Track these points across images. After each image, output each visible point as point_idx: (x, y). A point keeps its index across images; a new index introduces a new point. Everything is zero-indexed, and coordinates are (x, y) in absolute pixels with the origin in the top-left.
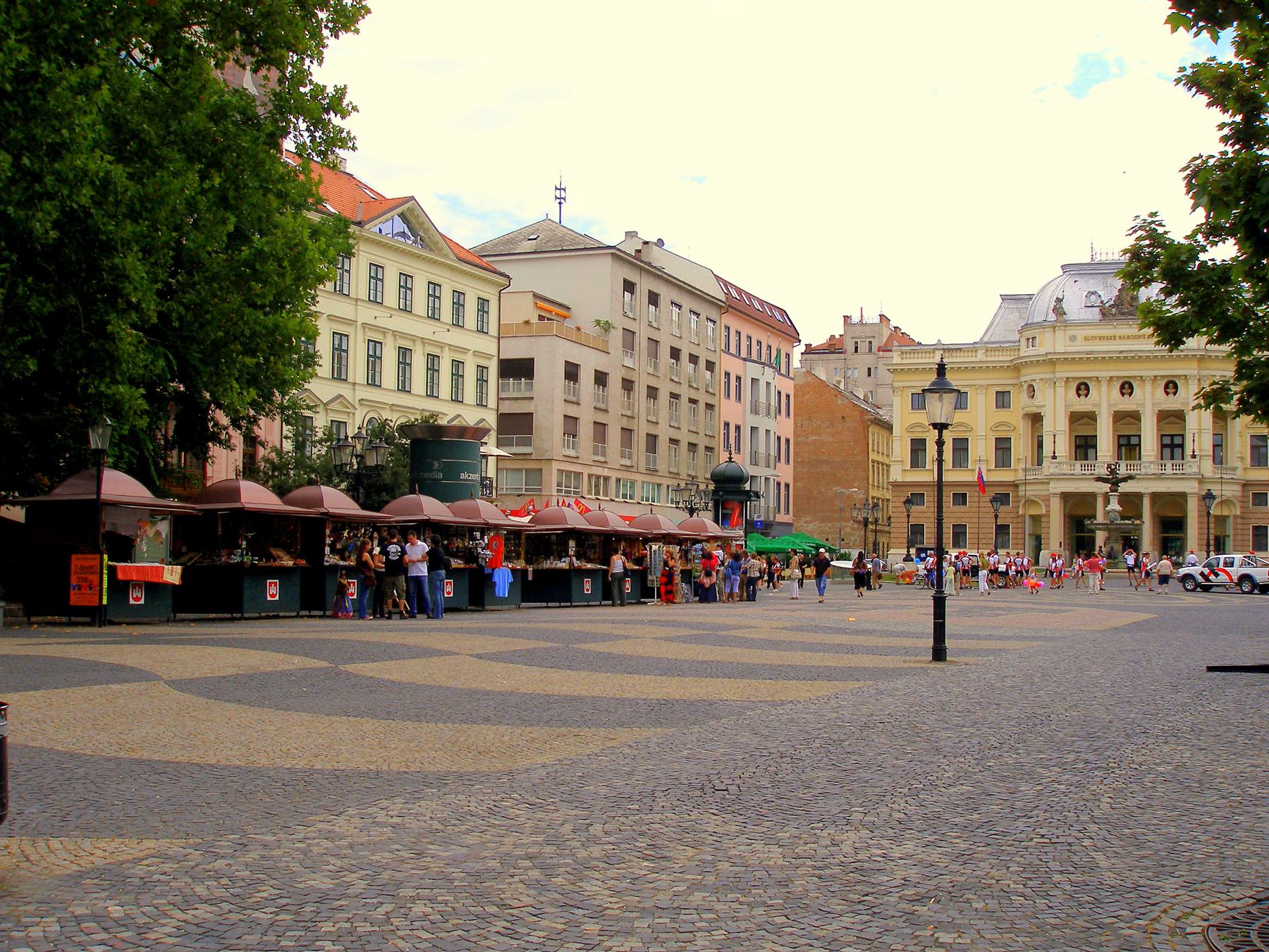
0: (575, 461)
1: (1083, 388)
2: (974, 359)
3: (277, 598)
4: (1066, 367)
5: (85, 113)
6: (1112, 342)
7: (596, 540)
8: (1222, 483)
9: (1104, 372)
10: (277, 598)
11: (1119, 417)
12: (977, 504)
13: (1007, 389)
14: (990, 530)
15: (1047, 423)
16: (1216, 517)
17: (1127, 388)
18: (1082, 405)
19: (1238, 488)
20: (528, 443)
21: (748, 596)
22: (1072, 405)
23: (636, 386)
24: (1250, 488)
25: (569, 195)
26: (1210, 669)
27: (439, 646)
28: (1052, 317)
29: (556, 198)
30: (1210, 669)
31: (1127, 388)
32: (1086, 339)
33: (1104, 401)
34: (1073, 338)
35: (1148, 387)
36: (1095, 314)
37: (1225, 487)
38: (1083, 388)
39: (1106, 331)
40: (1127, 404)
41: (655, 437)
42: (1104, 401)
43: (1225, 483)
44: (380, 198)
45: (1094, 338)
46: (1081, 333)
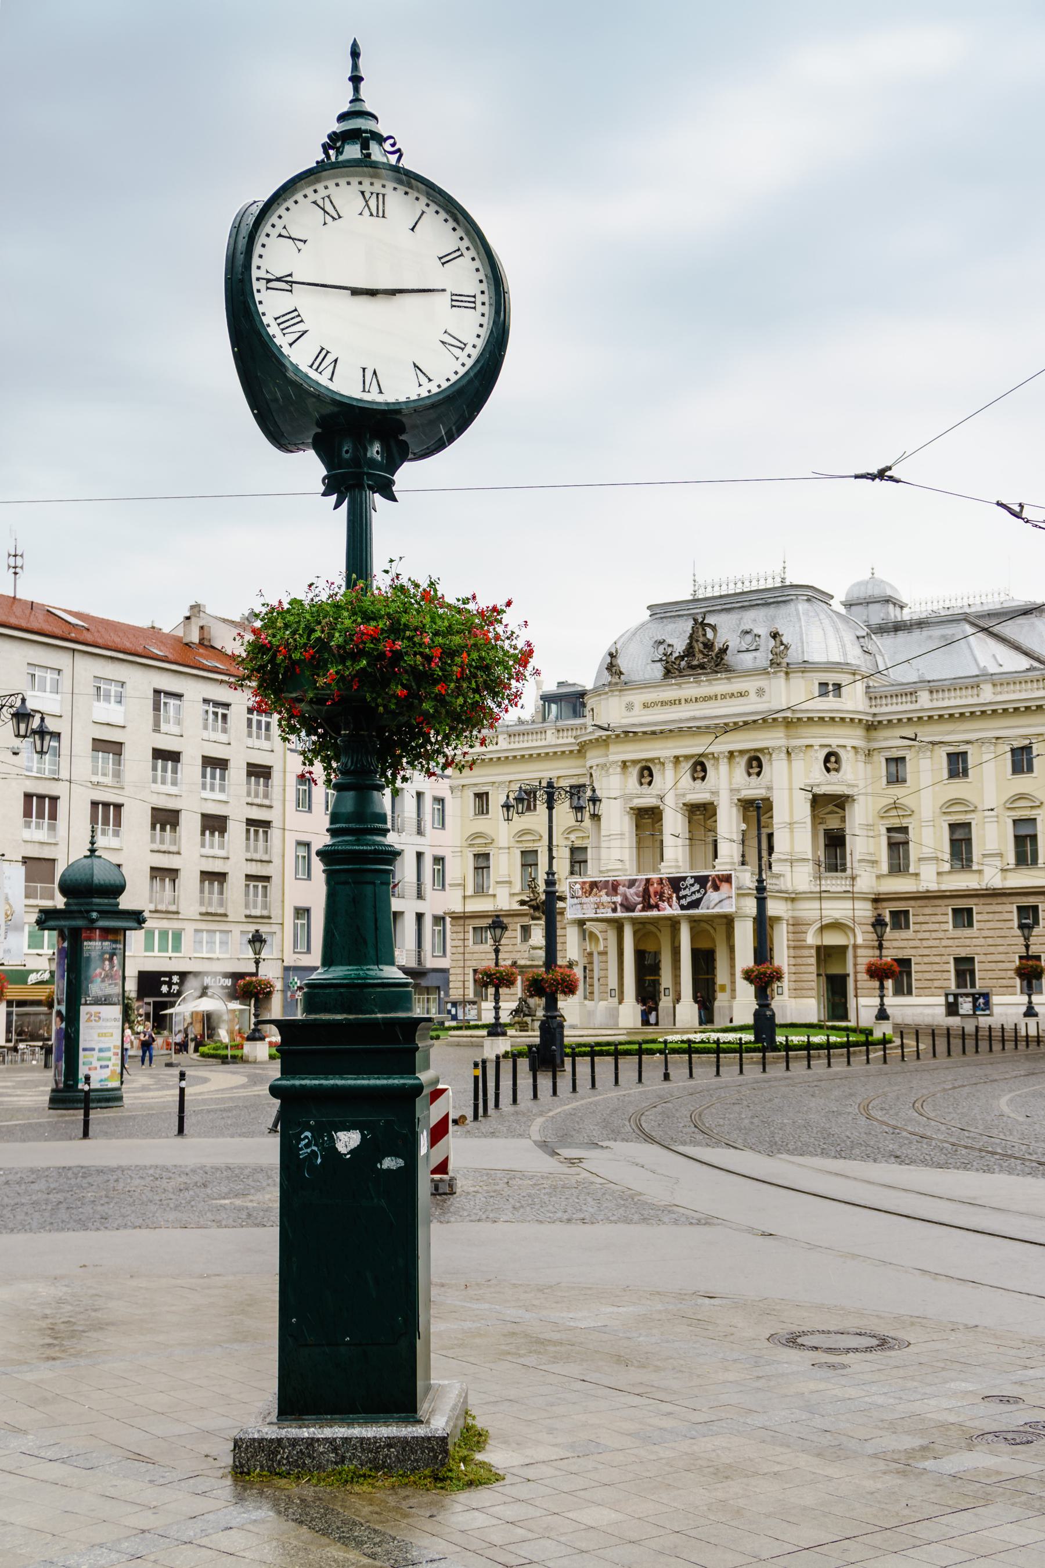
0: (175, 916)
2: (543, 743)
4: (620, 748)
6: (674, 708)
7: (843, 1000)
8: (820, 898)
9: (723, 745)
12: (461, 957)
13: (962, 748)
14: (920, 976)
15: (780, 815)
17: (699, 768)
19: (869, 905)
22: (738, 790)
24: (885, 904)
25: (27, 562)
27: (655, 1192)
28: (607, 677)
29: (9, 567)
32: (646, 706)
34: (630, 707)
35: (724, 766)
36: (658, 670)
37: (826, 904)
38: (646, 772)
39: (670, 693)
40: (699, 794)
43: (859, 898)
45: (655, 704)
46: (637, 698)
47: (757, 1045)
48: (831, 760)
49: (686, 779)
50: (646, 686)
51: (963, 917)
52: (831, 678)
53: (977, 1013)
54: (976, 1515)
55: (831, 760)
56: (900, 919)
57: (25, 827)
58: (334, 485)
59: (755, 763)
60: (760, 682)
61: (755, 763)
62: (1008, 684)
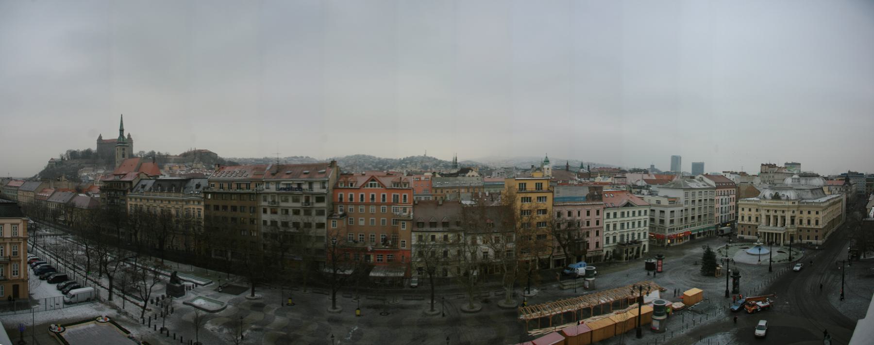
1: (768, 211)
3: (360, 218)
5: (546, 310)
9: (771, 209)
10: (360, 218)
11: (774, 216)
16: (122, 232)
17: (776, 211)
18: (768, 214)
20: (663, 224)
21: (120, 184)
23: (665, 221)
26: (122, 115)
30: (122, 115)
31: (776, 211)
33: (772, 214)
36: (770, 198)
38: (768, 211)
39: (772, 201)
41: (802, 220)
42: (772, 214)
44: (672, 200)
46: (768, 201)
47: (159, 271)
48: (793, 212)
49: (774, 212)
50: (768, 200)
51: (809, 231)
52: (794, 201)
53: (88, 277)
54: (544, 292)
55: (793, 212)
56: (801, 231)
57: (266, 221)
58: (102, 137)
59: (783, 212)
60: (785, 202)
61: (783, 212)
62: (194, 211)
